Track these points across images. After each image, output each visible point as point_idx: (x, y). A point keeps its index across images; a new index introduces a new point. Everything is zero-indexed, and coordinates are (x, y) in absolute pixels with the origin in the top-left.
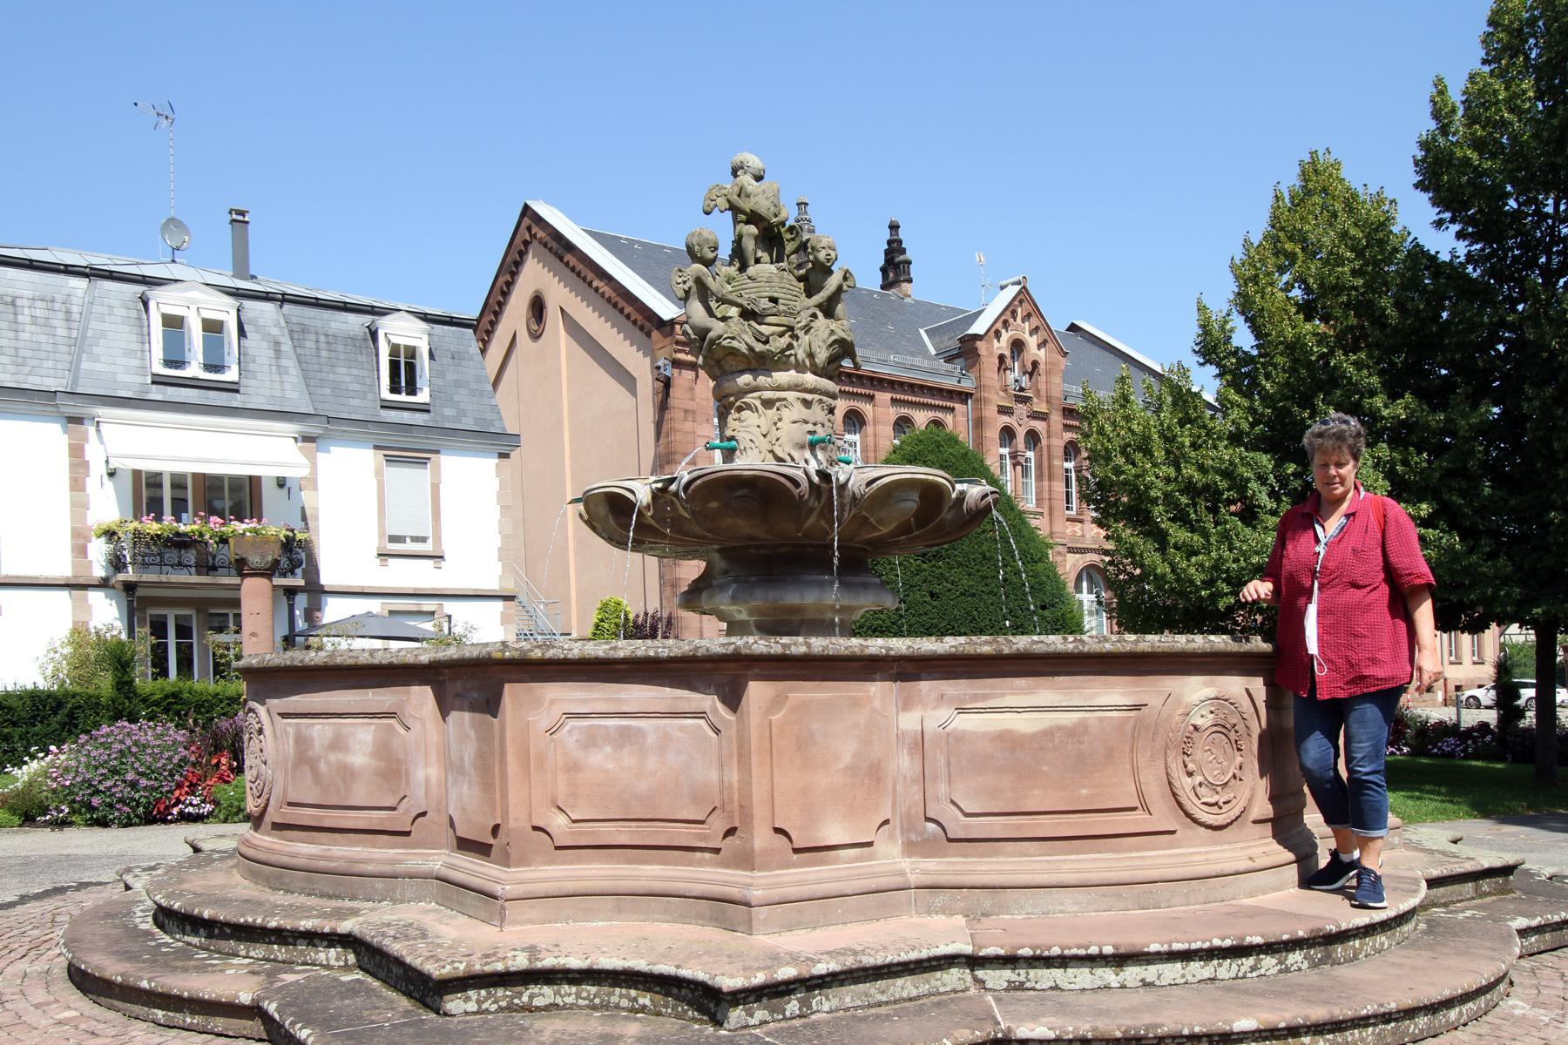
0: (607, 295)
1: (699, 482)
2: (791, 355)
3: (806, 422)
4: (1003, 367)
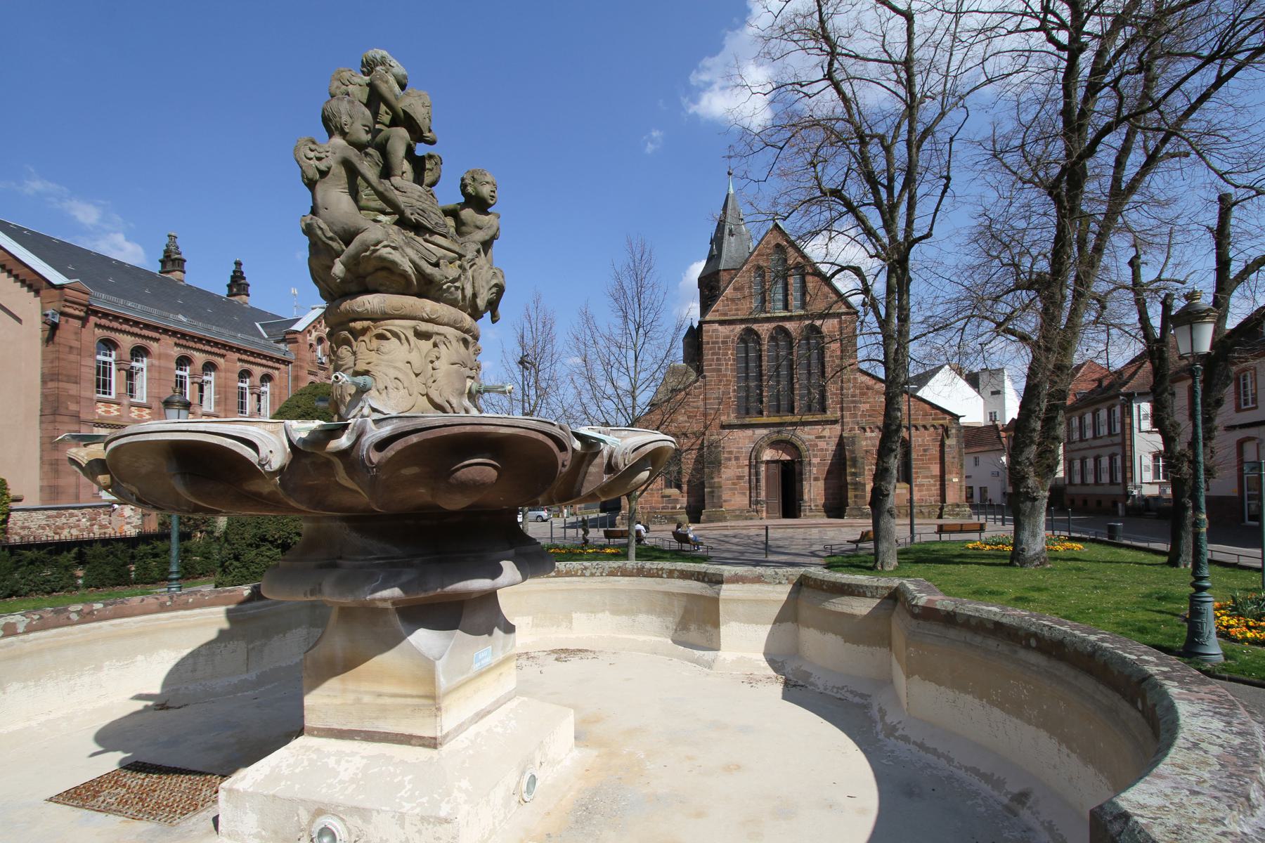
1: (414, 439)
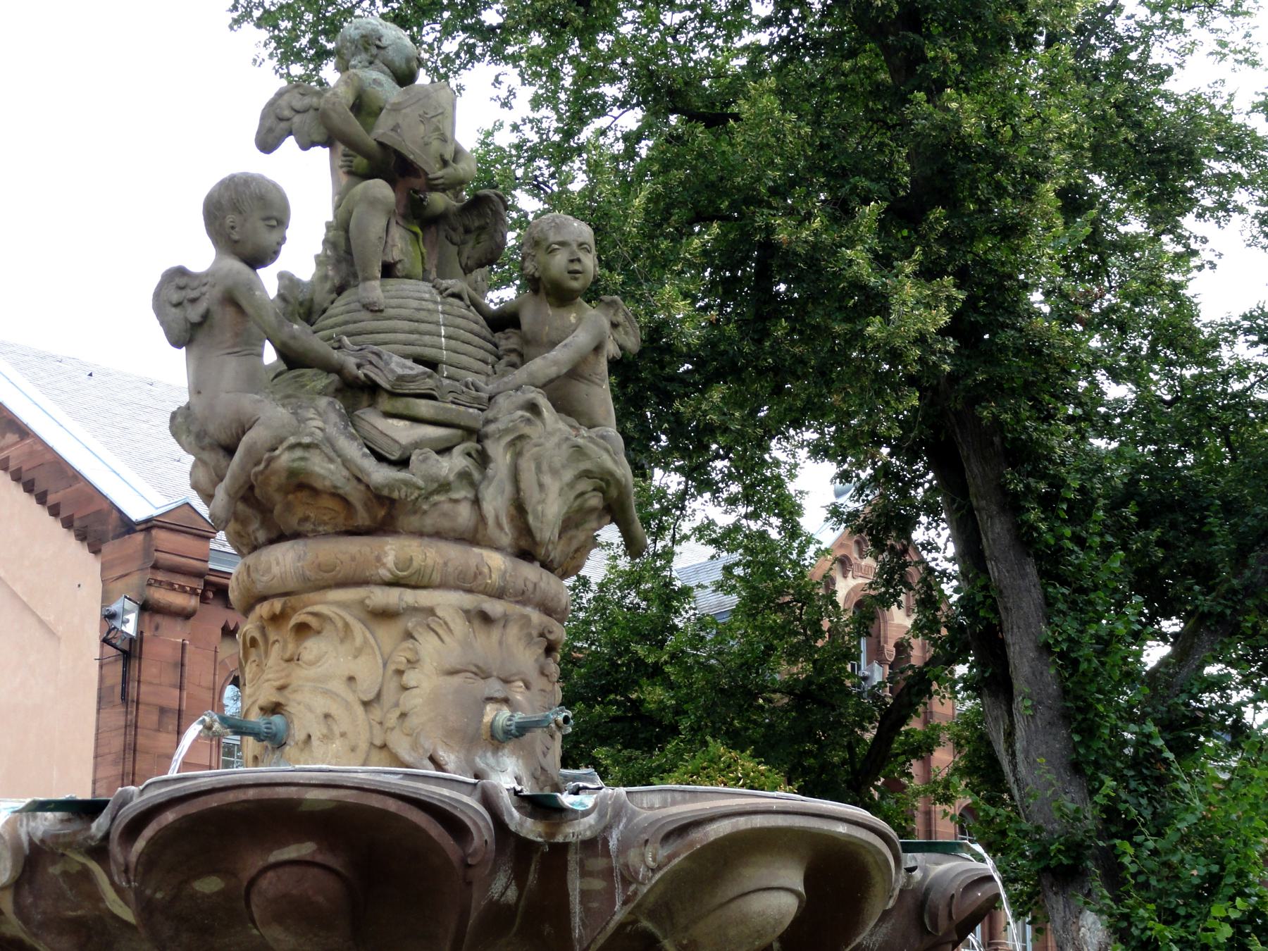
1: (170, 817)
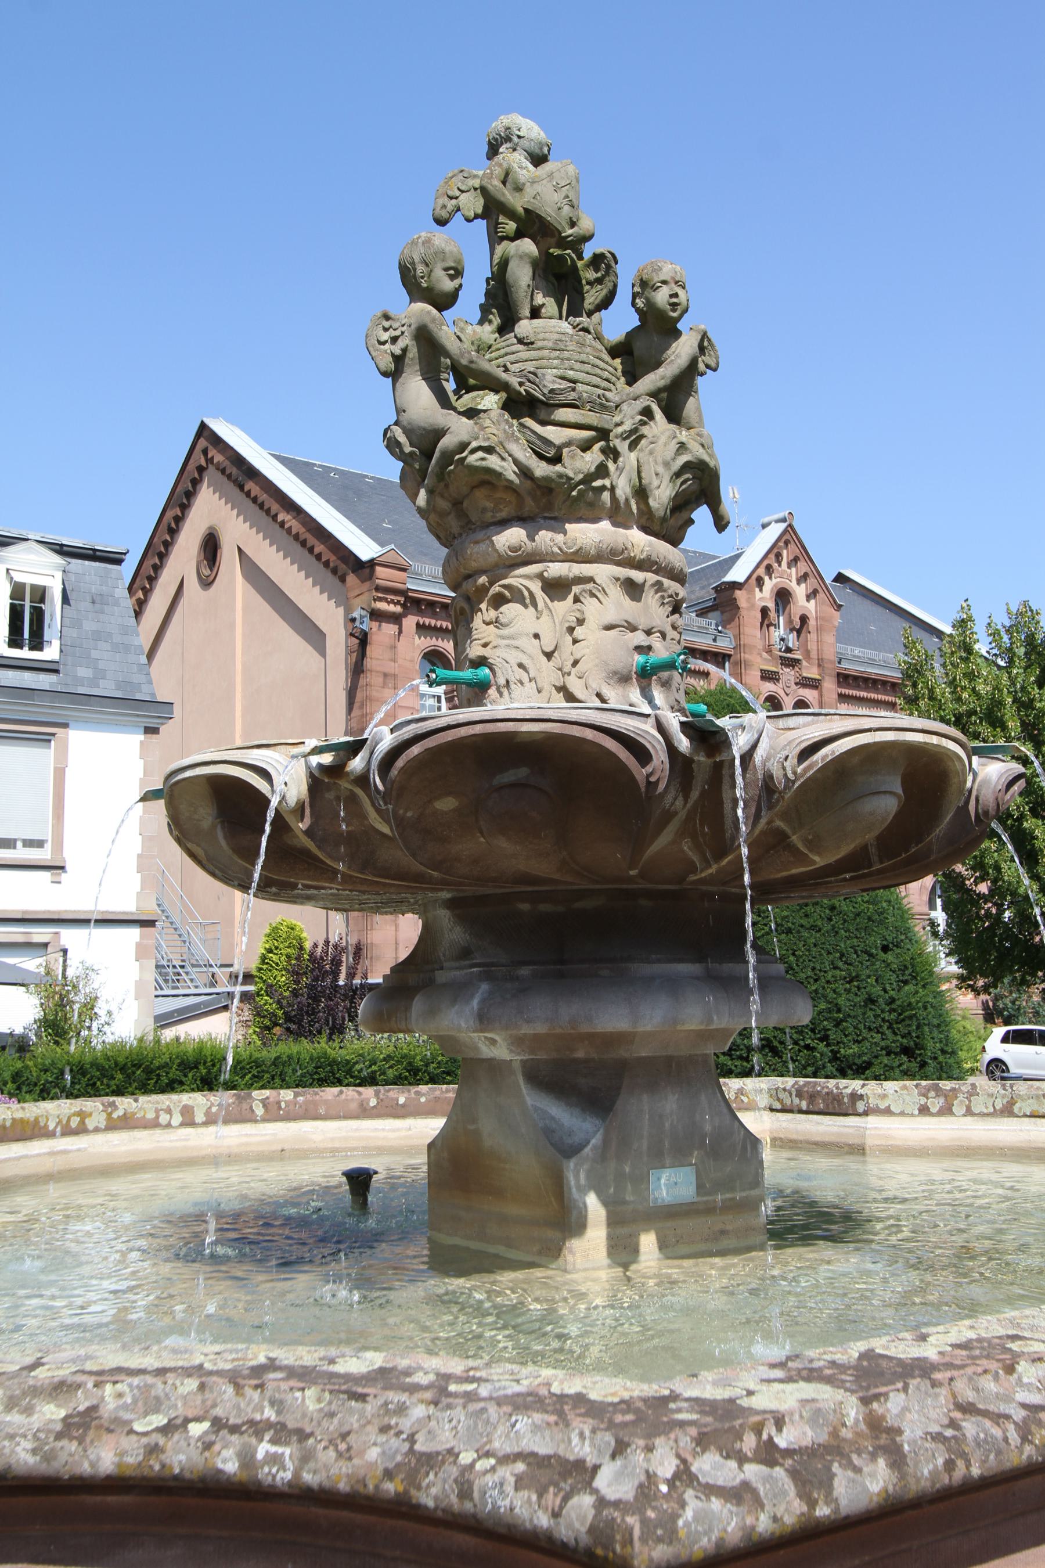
0: (294, 532)
1: (415, 750)
2: (603, 488)
3: (633, 628)
4: (766, 622)
